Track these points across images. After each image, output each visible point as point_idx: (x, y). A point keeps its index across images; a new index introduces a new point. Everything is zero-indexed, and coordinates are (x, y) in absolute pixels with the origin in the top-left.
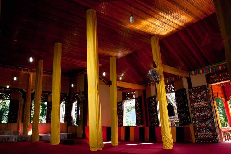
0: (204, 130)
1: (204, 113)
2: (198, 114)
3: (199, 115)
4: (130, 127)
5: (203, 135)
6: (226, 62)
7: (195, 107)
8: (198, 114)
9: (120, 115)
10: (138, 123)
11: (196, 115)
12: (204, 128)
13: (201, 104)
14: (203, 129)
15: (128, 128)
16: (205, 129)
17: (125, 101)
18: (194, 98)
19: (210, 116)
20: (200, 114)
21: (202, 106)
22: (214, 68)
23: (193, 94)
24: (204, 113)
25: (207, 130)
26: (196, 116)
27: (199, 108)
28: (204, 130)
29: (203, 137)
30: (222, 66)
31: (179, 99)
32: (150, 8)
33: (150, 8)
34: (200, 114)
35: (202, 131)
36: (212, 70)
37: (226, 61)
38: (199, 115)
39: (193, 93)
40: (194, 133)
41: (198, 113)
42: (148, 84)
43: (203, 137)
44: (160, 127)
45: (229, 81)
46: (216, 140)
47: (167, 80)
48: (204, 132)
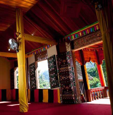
0: (67, 92)
1: (67, 77)
2: (63, 78)
3: (64, 79)
4: (43, 90)
5: (66, 96)
6: (98, 23)
7: (61, 71)
8: (63, 78)
9: (33, 78)
10: (52, 85)
11: (62, 79)
12: (67, 91)
13: (66, 69)
14: (66, 91)
15: (41, 91)
16: (68, 92)
17: (16, 68)
18: (60, 64)
19: (72, 79)
20: (65, 78)
21: (66, 71)
22: (76, 35)
23: (60, 60)
24: (67, 77)
25: (70, 92)
26: (61, 80)
27: (64, 72)
28: (68, 92)
29: (67, 98)
30: (82, 32)
31: (50, 65)
32: (16, 3)
33: (16, 3)
34: (65, 78)
35: (66, 93)
36: (75, 37)
37: (98, 22)
38: (64, 79)
39: (59, 59)
40: (60, 95)
41: (63, 77)
42: (30, 53)
43: (67, 98)
44: (17, 90)
45: (102, 42)
46: (76, 102)
47: (35, 52)
48: (67, 94)
